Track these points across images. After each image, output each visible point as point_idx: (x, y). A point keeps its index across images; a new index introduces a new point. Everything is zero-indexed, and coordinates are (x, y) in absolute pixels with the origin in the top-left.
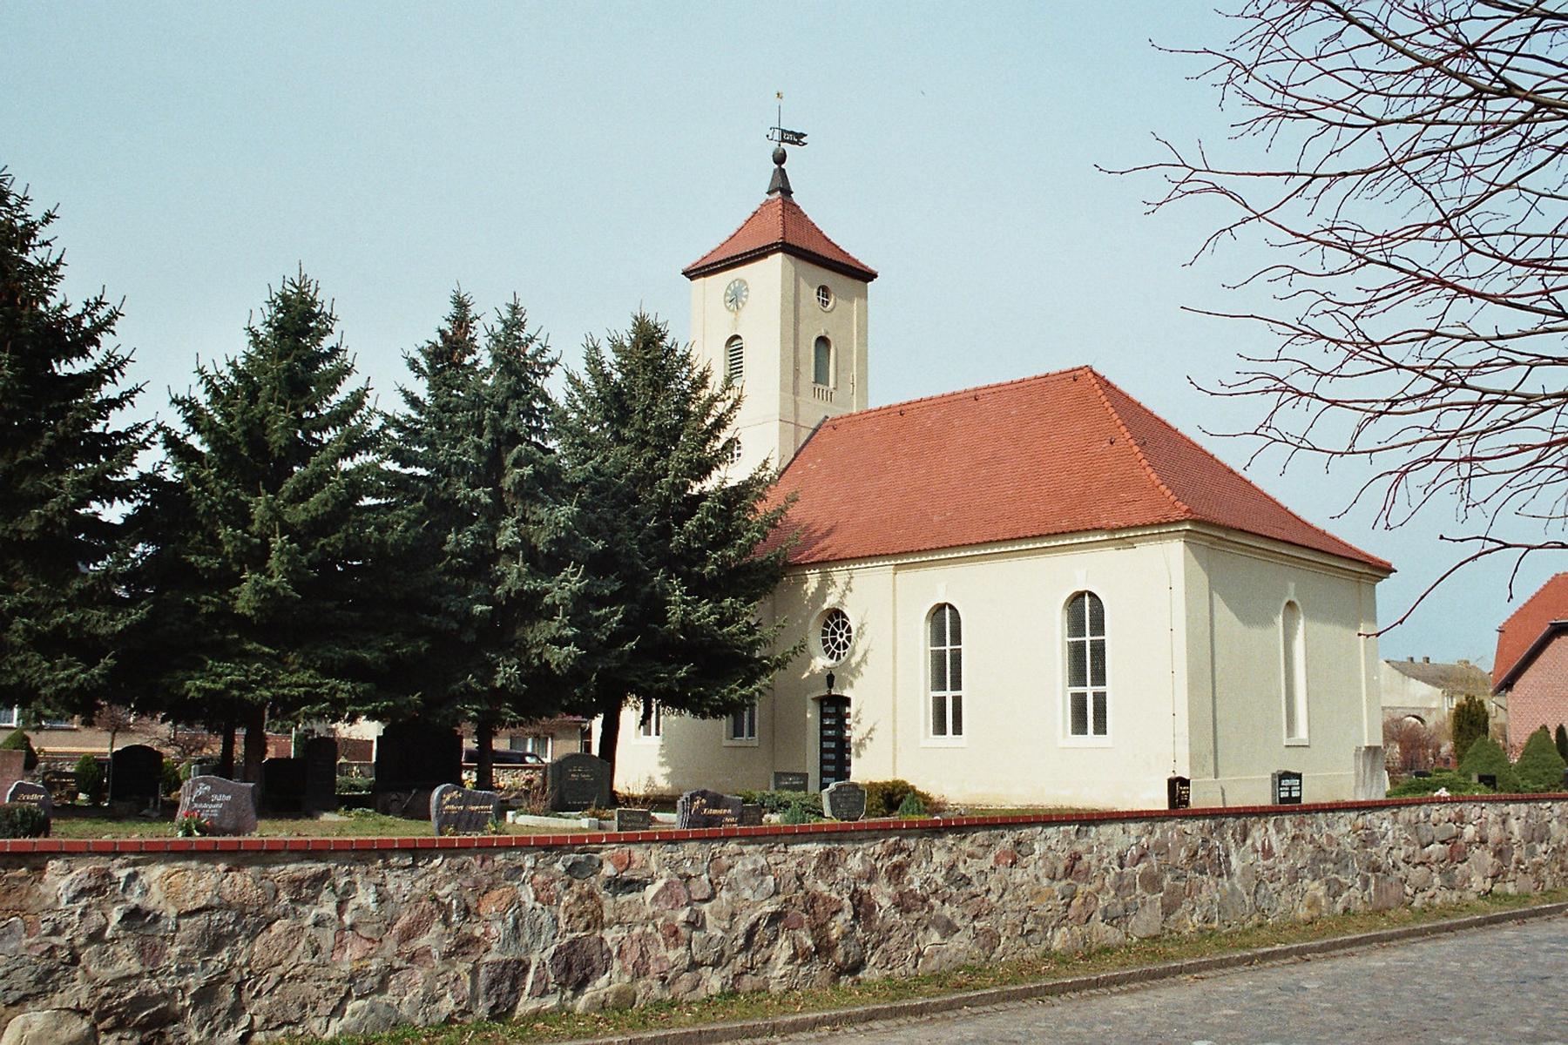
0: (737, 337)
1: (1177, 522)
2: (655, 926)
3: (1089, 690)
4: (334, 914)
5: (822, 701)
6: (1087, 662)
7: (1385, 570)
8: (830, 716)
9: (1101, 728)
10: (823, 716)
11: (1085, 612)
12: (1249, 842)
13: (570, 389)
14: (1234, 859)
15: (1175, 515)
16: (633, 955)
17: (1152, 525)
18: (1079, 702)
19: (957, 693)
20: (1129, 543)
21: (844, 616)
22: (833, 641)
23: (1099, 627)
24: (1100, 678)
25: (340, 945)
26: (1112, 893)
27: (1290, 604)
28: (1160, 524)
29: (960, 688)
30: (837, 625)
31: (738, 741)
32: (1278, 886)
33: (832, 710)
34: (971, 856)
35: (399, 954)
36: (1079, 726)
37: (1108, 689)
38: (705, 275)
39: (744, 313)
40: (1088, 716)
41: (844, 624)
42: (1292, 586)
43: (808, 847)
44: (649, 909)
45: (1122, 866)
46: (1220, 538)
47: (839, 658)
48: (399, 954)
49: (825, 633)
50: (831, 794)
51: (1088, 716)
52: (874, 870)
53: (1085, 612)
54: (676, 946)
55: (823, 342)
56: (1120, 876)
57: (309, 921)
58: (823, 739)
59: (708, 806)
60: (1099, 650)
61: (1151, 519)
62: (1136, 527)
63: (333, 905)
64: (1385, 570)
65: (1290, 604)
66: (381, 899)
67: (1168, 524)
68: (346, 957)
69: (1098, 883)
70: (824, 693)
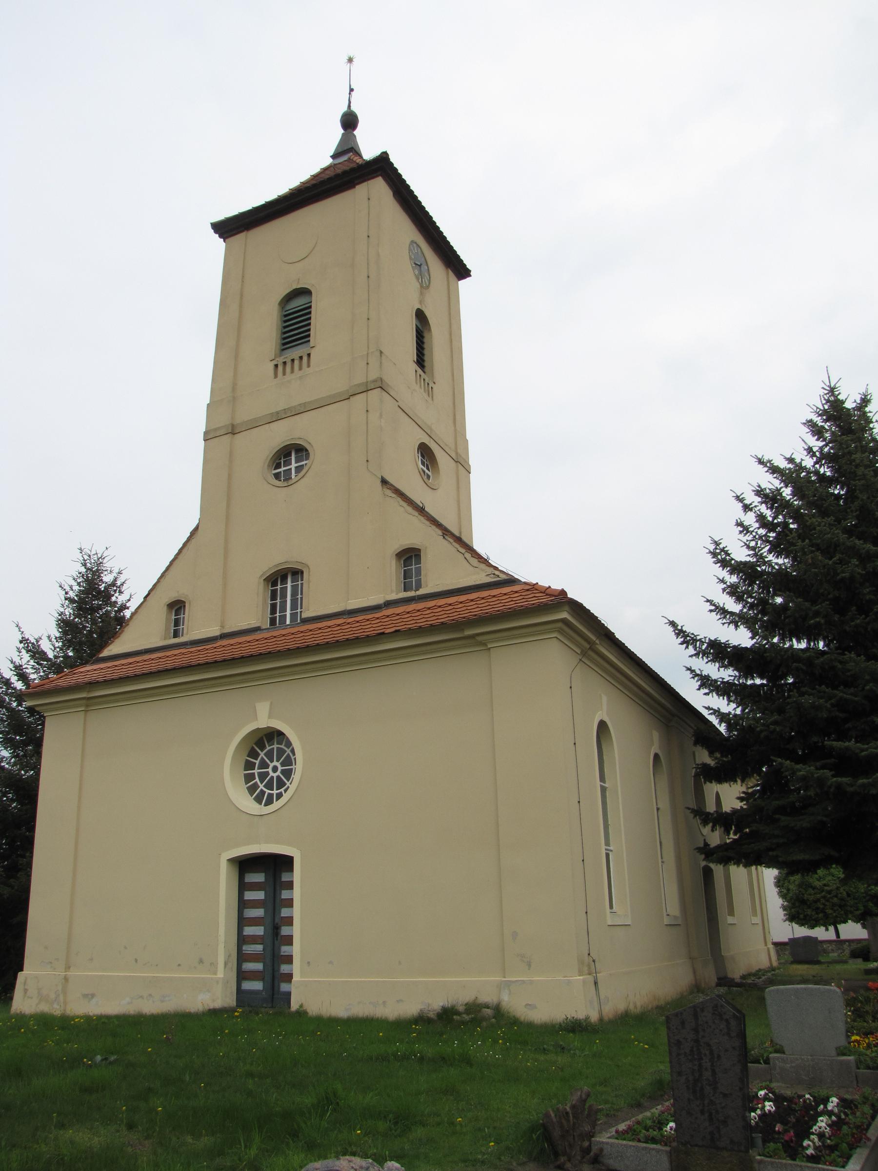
12: (707, 1115)
30: (270, 755)
41: (281, 752)
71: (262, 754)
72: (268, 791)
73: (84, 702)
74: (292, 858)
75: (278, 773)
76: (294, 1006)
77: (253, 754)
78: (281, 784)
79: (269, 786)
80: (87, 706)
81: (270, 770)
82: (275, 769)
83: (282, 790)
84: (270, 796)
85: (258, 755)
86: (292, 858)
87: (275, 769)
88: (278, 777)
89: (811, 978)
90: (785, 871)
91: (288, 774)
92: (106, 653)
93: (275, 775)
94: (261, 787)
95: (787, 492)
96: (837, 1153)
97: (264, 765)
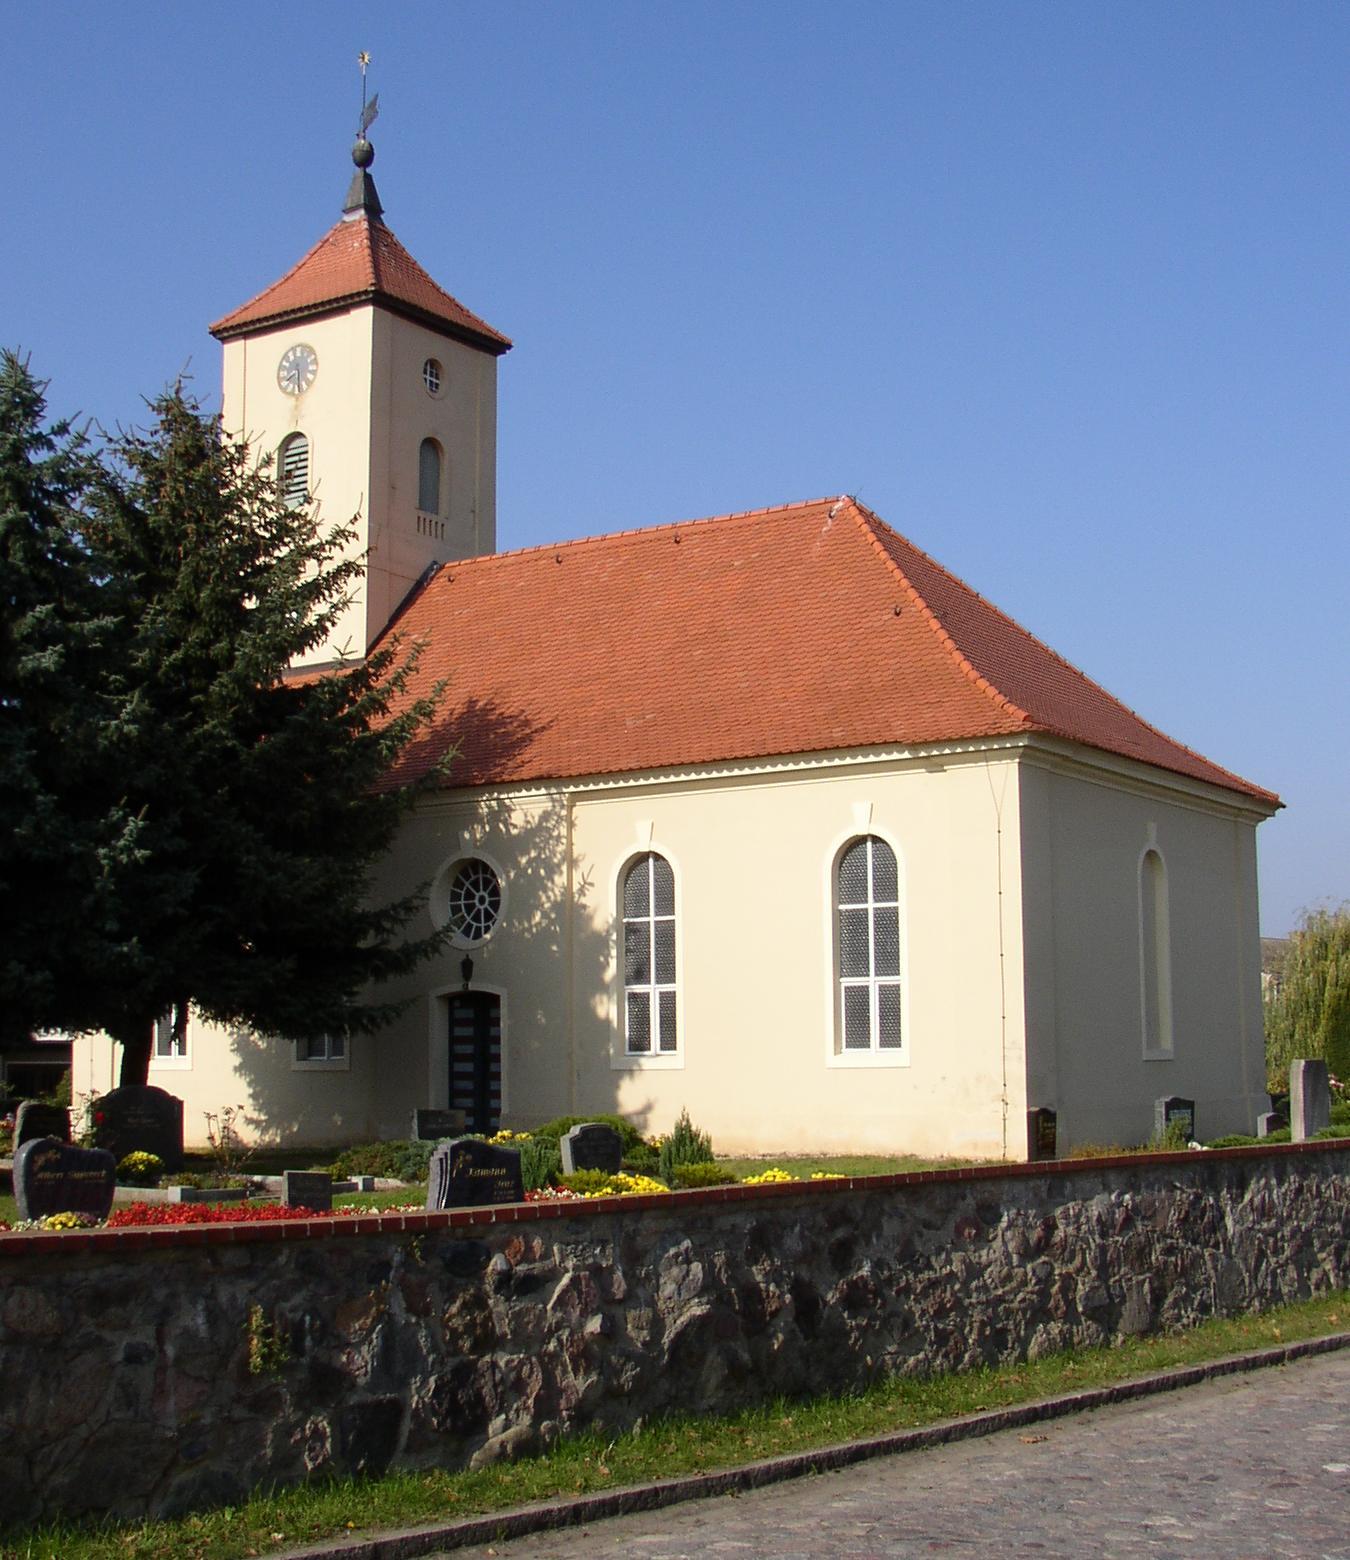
0: (299, 435)
1: (1012, 735)
2: (560, 1341)
3: (873, 982)
4: (152, 1343)
5: (451, 1000)
6: (866, 938)
7: (1268, 805)
8: (464, 1023)
9: (891, 1037)
10: (453, 1022)
11: (863, 866)
13: (307, 509)
14: (1229, 1222)
15: (1007, 725)
16: (535, 1386)
17: (974, 739)
18: (857, 1002)
19: (667, 987)
20: (935, 765)
21: (486, 868)
22: (470, 908)
23: (888, 886)
24: (889, 961)
25: (160, 1391)
26: (1094, 1273)
27: (1151, 854)
28: (986, 738)
29: (672, 980)
30: (475, 885)
31: (855, 1056)
32: (1282, 1258)
33: (469, 1013)
34: (928, 1225)
35: (238, 1399)
36: (857, 1035)
37: (904, 980)
38: (246, 335)
39: (312, 397)
40: (869, 1020)
42: (1152, 827)
43: (738, 1219)
44: (552, 1318)
45: (1103, 1235)
46: (1066, 758)
47: (478, 935)
48: (238, 1399)
49: (455, 897)
50: (574, 1142)
51: (869, 1020)
52: (815, 1249)
53: (863, 866)
54: (587, 1373)
55: (431, 445)
56: (1103, 1249)
57: (119, 1356)
58: (454, 1058)
59: (476, 1166)
60: (888, 923)
61: (981, 730)
62: (950, 741)
63: (151, 1330)
64: (1268, 805)
65: (1151, 854)
66: (213, 1317)
67: (999, 736)
68: (171, 1406)
69: (1077, 1261)
70: (457, 987)
71: (467, 884)
72: (475, 924)
73: (1236, 811)
74: (498, 997)
75: (477, 895)
76: (103, 1030)
77: (458, 884)
78: (489, 917)
79: (477, 918)
80: (1237, 816)
81: (476, 901)
82: (482, 900)
83: (490, 923)
84: (478, 929)
85: (463, 885)
86: (498, 997)
87: (482, 900)
88: (486, 910)
89: (632, 958)
90: (517, 853)
91: (495, 905)
92: (291, 447)
93: (482, 907)
94: (469, 919)
95: (377, 723)
96: (933, 1259)
97: (469, 896)
